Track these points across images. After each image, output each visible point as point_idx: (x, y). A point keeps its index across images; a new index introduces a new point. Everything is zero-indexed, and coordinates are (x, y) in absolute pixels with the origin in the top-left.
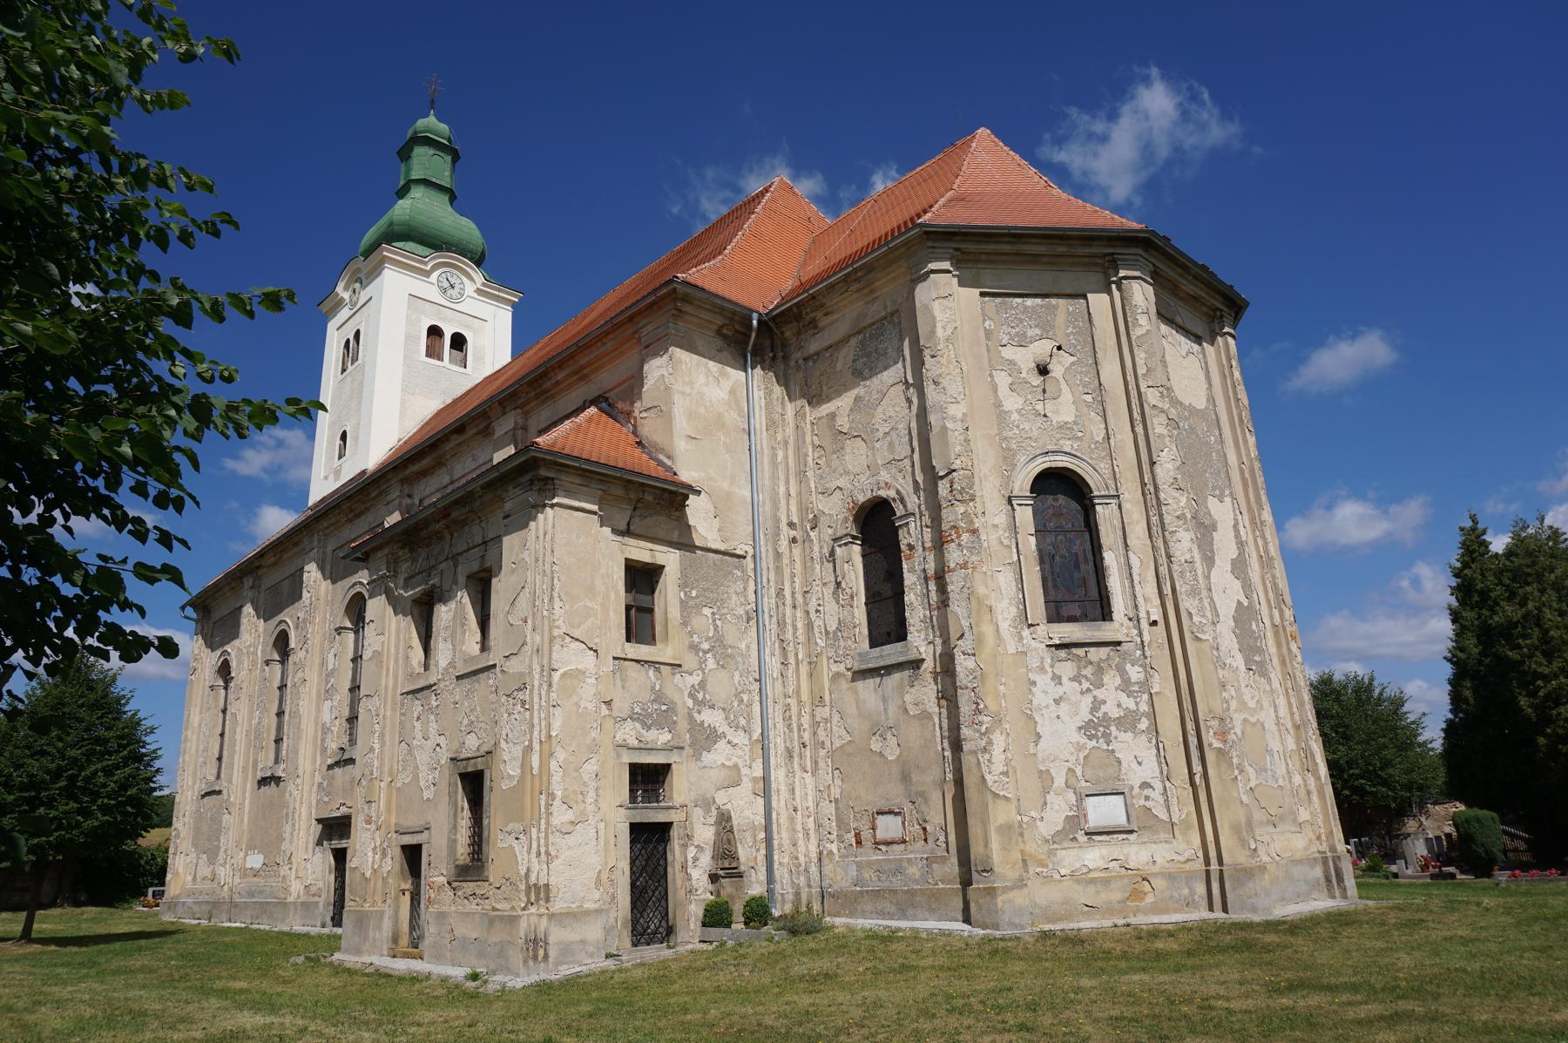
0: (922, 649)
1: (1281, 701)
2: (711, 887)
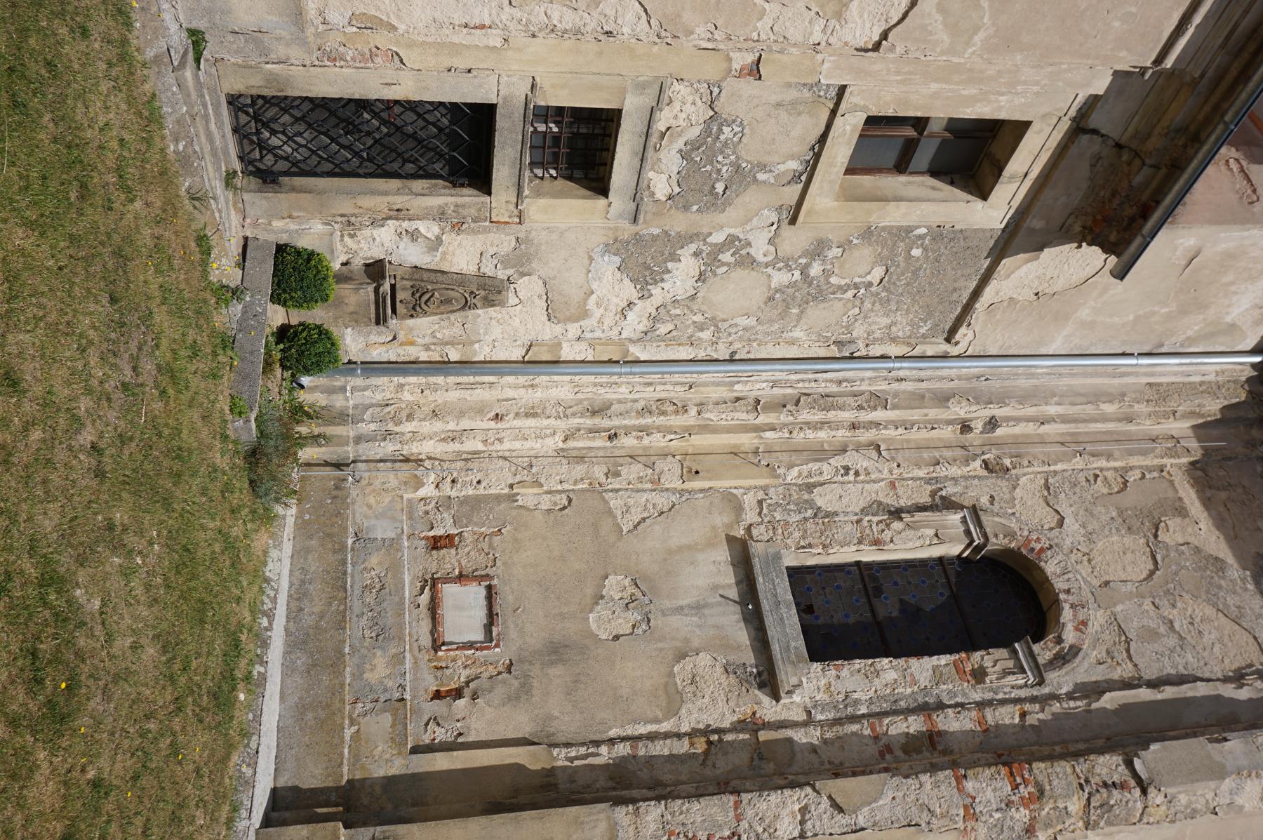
0: (796, 698)
2: (358, 263)
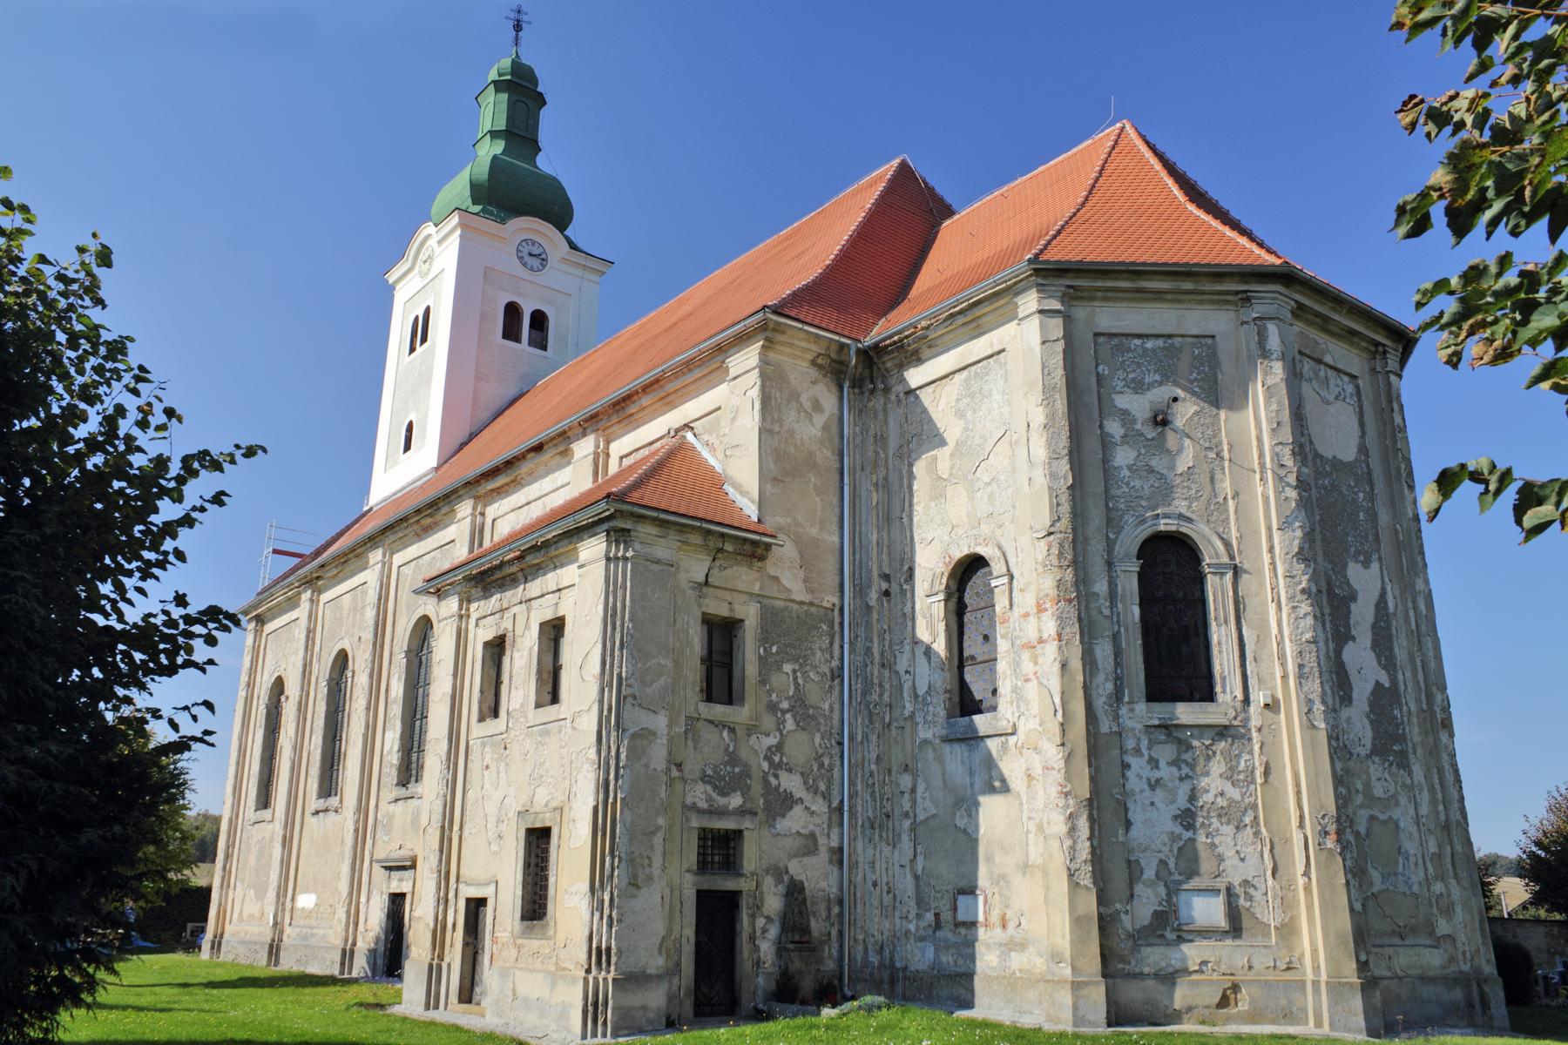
1: (1425, 797)
2: (1220, 850)
